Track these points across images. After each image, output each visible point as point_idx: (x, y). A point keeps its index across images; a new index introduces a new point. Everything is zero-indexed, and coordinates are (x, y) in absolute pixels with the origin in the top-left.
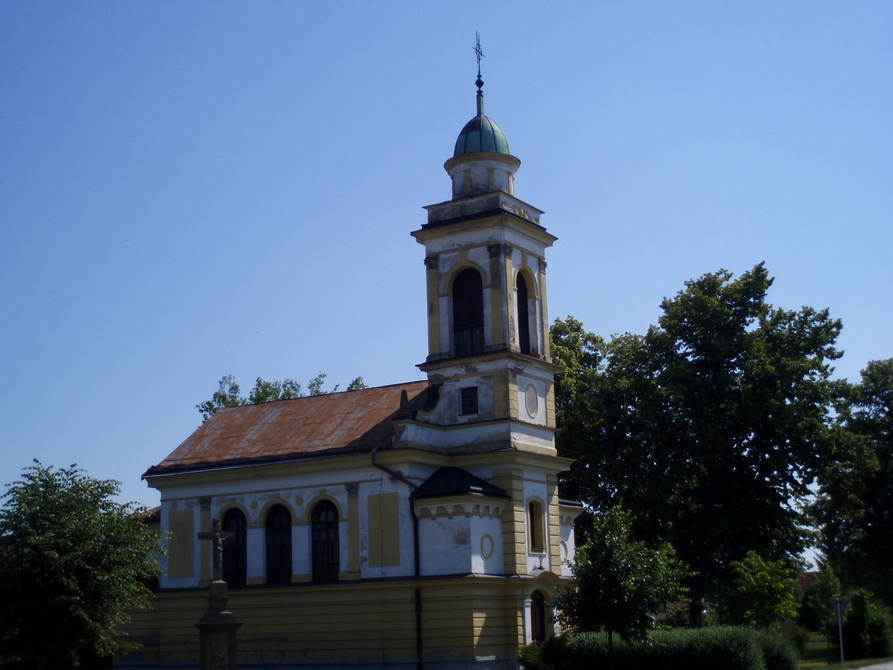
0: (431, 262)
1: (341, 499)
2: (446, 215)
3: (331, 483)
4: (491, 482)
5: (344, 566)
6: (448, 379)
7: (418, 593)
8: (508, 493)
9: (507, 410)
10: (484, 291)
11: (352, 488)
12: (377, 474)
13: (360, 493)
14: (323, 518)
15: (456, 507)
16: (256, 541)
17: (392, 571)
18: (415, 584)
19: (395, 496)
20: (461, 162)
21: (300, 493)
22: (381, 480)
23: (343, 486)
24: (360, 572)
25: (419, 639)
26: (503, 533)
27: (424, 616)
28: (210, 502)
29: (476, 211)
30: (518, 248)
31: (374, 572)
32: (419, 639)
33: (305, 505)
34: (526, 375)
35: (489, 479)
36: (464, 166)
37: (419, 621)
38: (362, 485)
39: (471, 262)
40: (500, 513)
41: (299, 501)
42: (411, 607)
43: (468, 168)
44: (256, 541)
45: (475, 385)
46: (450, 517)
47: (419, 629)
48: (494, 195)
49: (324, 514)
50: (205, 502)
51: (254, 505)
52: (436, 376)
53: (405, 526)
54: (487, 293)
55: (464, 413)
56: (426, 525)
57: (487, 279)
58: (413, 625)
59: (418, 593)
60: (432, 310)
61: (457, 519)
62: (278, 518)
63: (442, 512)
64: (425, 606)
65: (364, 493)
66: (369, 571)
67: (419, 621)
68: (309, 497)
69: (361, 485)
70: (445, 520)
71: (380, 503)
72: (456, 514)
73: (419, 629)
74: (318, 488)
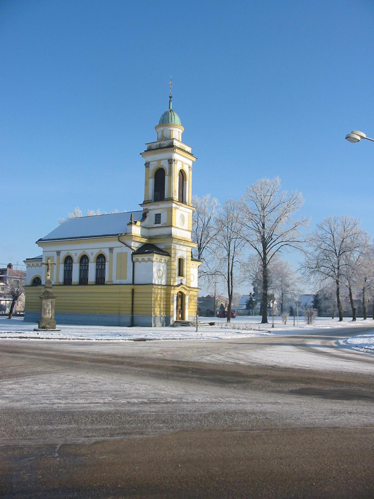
0: (147, 165)
1: (107, 253)
2: (154, 146)
3: (102, 247)
4: (164, 250)
5: (107, 279)
6: (150, 210)
7: (133, 290)
8: (170, 254)
9: (172, 223)
10: (166, 177)
11: (111, 249)
12: (120, 244)
13: (114, 252)
14: (84, 261)
15: (33, 264)
16: (76, 268)
17: (124, 281)
18: (132, 287)
19: (126, 253)
20: (161, 127)
21: (92, 250)
22: (121, 247)
23: (56, 252)
24: (112, 281)
25: (133, 307)
26: (167, 269)
27: (135, 299)
28: (60, 253)
29: (165, 146)
30: (180, 161)
31: (118, 281)
32: (133, 307)
33: (94, 255)
34: (181, 210)
35: (163, 249)
36: (162, 128)
37: (133, 301)
38: (62, 252)
39: (162, 166)
40: (166, 262)
41: (76, 254)
42: (130, 295)
43: (163, 129)
44: (76, 268)
45: (160, 213)
46: (31, 267)
47: (133, 304)
48: (172, 140)
49: (101, 259)
50: (58, 253)
51: (76, 254)
52: (146, 209)
53: (130, 264)
54: (166, 178)
55: (156, 223)
56: (137, 264)
57: (167, 172)
58: (131, 302)
59: (133, 290)
60: (146, 183)
61: (148, 262)
62: (84, 259)
63: (143, 260)
64: (135, 295)
65: (115, 251)
66: (115, 281)
67: (133, 301)
68: (96, 252)
69: (114, 248)
70: (144, 263)
71: (120, 255)
72: (142, 261)
73: (133, 304)
74: (99, 249)
